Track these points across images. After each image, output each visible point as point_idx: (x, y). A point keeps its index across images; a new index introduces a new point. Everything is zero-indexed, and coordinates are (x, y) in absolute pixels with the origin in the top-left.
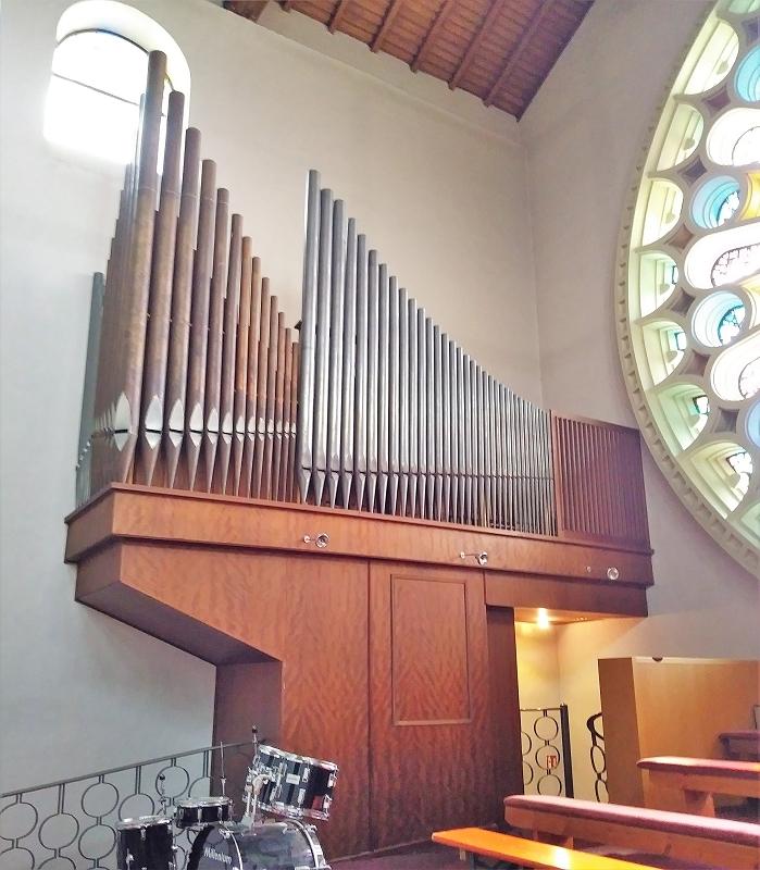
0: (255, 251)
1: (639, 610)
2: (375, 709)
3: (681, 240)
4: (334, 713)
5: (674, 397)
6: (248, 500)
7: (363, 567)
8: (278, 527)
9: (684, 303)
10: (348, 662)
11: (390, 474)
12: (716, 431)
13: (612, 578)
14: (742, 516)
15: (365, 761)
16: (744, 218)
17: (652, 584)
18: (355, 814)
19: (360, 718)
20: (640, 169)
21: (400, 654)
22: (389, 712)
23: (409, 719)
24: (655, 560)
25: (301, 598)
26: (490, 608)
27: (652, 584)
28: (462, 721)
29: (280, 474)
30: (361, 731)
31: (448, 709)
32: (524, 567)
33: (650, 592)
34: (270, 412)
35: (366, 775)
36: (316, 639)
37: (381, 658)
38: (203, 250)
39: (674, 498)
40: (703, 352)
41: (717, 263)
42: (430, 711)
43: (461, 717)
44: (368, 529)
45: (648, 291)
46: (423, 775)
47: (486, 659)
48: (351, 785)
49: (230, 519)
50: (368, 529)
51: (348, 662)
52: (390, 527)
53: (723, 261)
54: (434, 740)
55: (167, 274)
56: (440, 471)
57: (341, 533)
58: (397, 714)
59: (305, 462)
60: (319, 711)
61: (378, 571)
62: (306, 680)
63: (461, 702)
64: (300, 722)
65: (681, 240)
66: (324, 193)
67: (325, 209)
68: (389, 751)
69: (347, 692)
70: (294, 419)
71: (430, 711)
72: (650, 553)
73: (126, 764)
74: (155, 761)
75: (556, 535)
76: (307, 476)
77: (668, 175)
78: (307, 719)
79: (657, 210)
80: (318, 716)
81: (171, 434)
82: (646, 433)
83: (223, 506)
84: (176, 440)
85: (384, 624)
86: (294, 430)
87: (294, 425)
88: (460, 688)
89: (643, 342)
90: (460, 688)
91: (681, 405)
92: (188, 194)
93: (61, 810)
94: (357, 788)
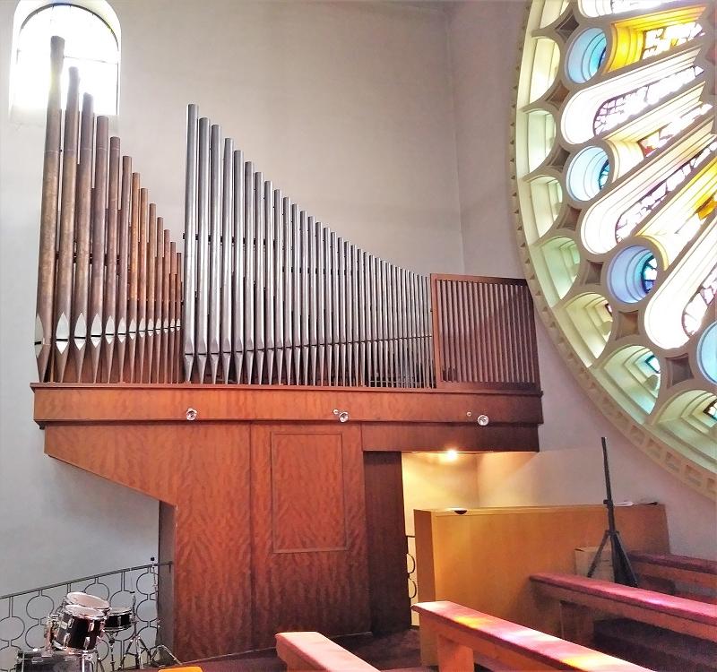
0: (142, 183)
1: (532, 445)
2: (257, 540)
3: (558, 97)
4: (220, 544)
5: (559, 248)
6: (150, 385)
7: (244, 427)
8: (160, 402)
9: (561, 157)
10: (232, 504)
11: (265, 351)
12: (587, 282)
13: (482, 423)
14: (604, 365)
15: (248, 583)
16: (611, 70)
17: (543, 423)
18: (239, 622)
19: (244, 547)
20: (524, 28)
21: (280, 495)
22: (269, 543)
23: (288, 548)
24: (544, 399)
25: (191, 456)
26: (366, 453)
27: (543, 423)
28: (337, 549)
29: (170, 361)
30: (244, 558)
31: (325, 539)
32: (399, 418)
33: (541, 429)
34: (159, 312)
35: (249, 591)
36: (203, 488)
37: (261, 502)
38: (99, 188)
39: (554, 347)
40: (578, 207)
41: (598, 114)
42: (308, 542)
43: (337, 545)
44: (246, 398)
45: (533, 153)
46: (301, 592)
47: (363, 497)
48: (235, 601)
49: (125, 401)
50: (246, 398)
51: (232, 504)
52: (265, 394)
53: (603, 111)
54: (311, 563)
55: (70, 216)
56: (322, 341)
57: (217, 402)
58: (279, 543)
59: (189, 349)
60: (208, 544)
61: (260, 432)
62: (195, 520)
63: (337, 534)
64: (191, 551)
65: (558, 97)
66: (202, 122)
67: (202, 135)
68: (269, 572)
69: (231, 528)
70: (179, 315)
71: (308, 542)
72: (541, 394)
73: (611, 478)
74: (141, 568)
75: (435, 387)
76: (189, 361)
77: (547, 32)
78: (197, 548)
79: (537, 74)
80: (206, 547)
81: (76, 340)
82: (531, 284)
83: (119, 391)
84: (110, 340)
85: (265, 472)
86: (178, 324)
87: (179, 321)
88: (338, 523)
89: (531, 197)
90: (338, 523)
91: (566, 255)
92: (85, 149)
93: (123, 589)
94: (240, 598)
